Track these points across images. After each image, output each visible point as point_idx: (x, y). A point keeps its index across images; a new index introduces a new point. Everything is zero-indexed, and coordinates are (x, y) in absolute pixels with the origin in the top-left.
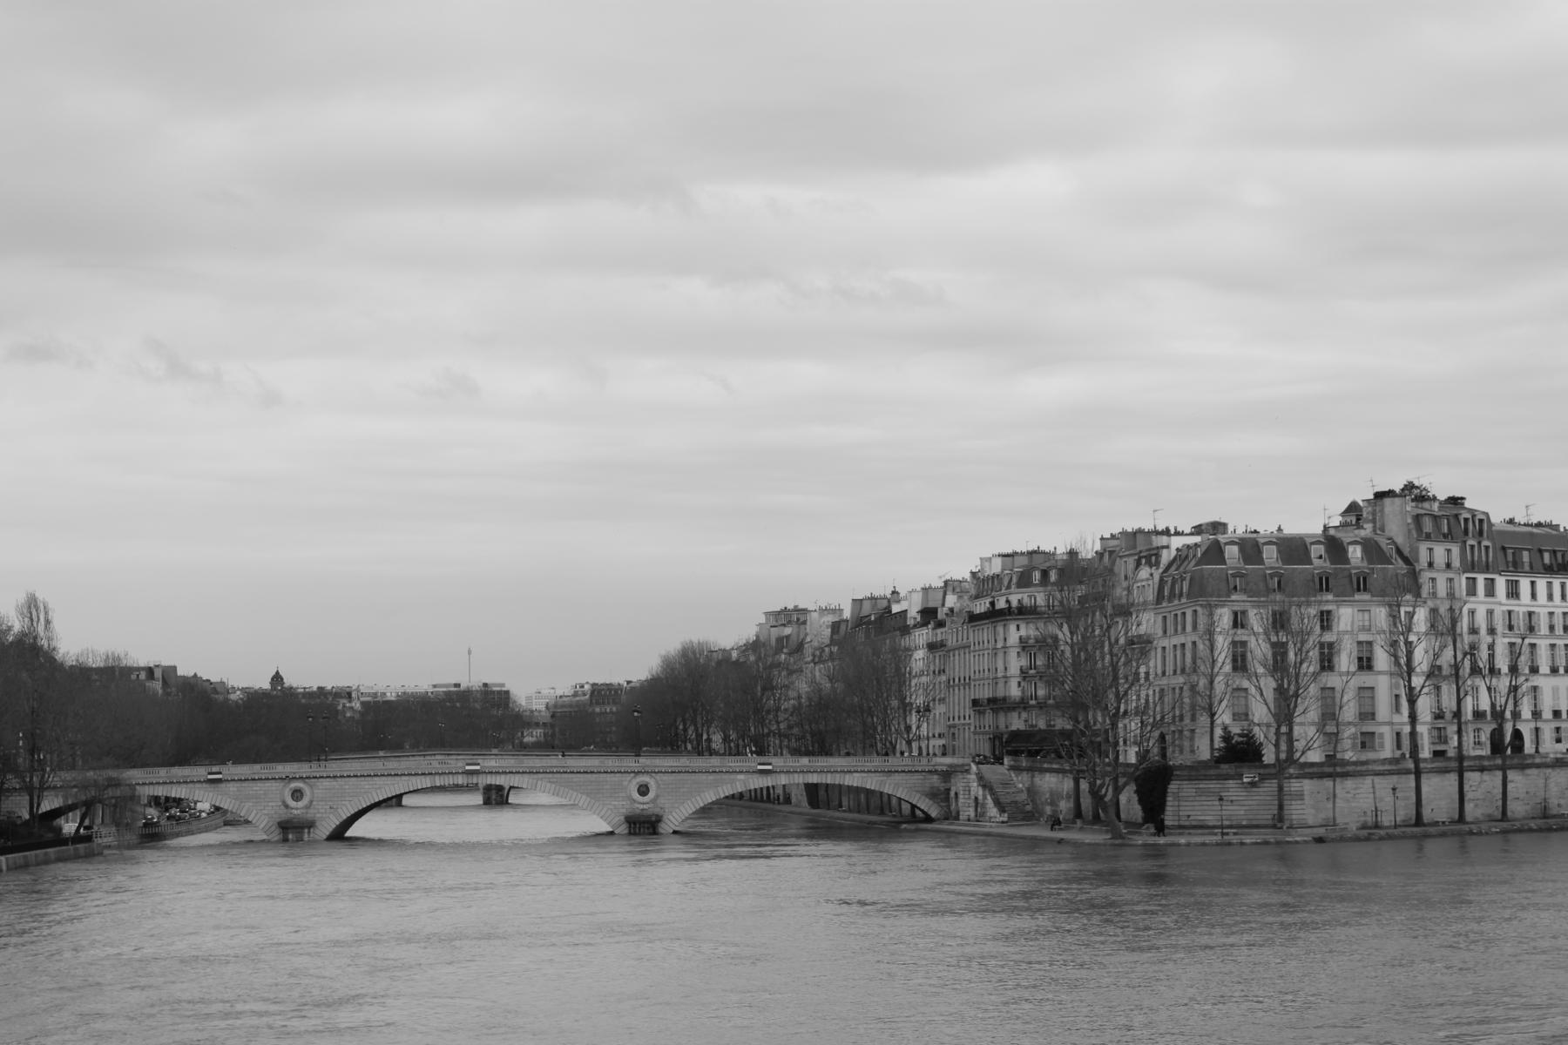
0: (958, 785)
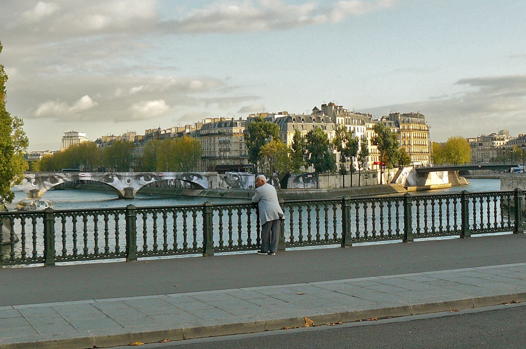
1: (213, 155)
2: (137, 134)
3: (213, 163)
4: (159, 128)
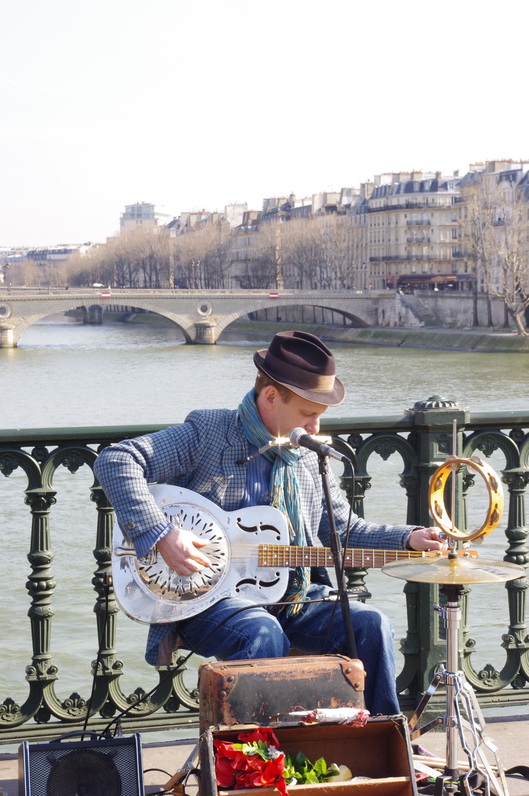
0: (385, 305)
1: (393, 253)
2: (249, 209)
3: (393, 269)
4: (292, 195)
